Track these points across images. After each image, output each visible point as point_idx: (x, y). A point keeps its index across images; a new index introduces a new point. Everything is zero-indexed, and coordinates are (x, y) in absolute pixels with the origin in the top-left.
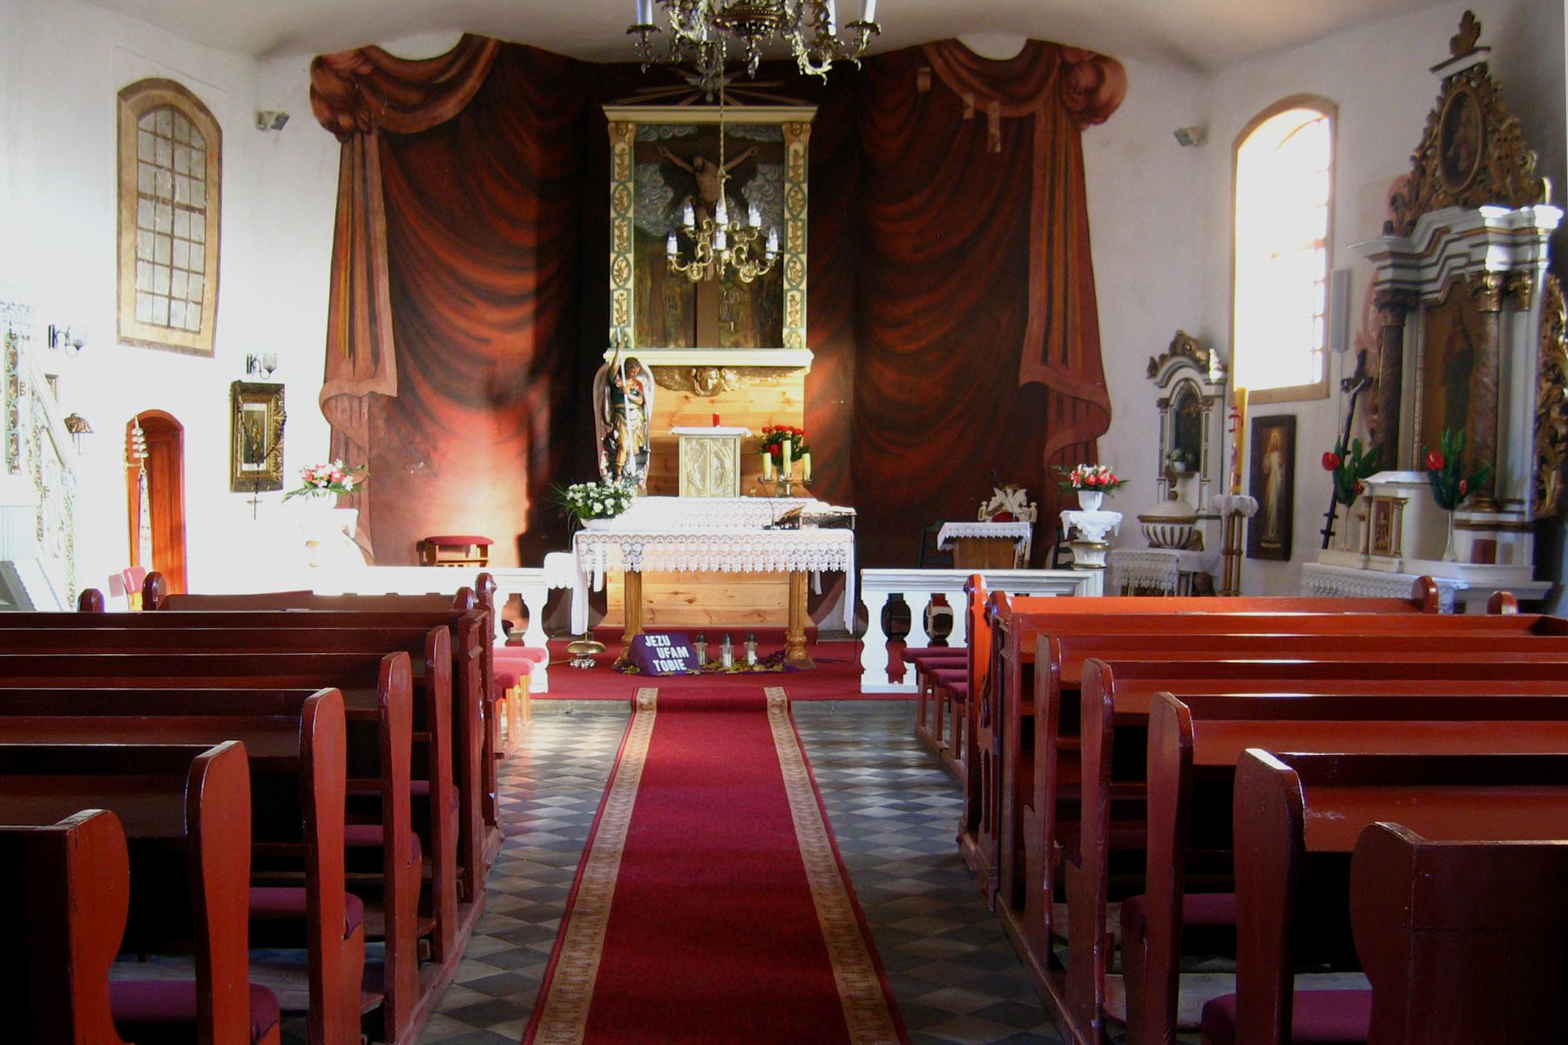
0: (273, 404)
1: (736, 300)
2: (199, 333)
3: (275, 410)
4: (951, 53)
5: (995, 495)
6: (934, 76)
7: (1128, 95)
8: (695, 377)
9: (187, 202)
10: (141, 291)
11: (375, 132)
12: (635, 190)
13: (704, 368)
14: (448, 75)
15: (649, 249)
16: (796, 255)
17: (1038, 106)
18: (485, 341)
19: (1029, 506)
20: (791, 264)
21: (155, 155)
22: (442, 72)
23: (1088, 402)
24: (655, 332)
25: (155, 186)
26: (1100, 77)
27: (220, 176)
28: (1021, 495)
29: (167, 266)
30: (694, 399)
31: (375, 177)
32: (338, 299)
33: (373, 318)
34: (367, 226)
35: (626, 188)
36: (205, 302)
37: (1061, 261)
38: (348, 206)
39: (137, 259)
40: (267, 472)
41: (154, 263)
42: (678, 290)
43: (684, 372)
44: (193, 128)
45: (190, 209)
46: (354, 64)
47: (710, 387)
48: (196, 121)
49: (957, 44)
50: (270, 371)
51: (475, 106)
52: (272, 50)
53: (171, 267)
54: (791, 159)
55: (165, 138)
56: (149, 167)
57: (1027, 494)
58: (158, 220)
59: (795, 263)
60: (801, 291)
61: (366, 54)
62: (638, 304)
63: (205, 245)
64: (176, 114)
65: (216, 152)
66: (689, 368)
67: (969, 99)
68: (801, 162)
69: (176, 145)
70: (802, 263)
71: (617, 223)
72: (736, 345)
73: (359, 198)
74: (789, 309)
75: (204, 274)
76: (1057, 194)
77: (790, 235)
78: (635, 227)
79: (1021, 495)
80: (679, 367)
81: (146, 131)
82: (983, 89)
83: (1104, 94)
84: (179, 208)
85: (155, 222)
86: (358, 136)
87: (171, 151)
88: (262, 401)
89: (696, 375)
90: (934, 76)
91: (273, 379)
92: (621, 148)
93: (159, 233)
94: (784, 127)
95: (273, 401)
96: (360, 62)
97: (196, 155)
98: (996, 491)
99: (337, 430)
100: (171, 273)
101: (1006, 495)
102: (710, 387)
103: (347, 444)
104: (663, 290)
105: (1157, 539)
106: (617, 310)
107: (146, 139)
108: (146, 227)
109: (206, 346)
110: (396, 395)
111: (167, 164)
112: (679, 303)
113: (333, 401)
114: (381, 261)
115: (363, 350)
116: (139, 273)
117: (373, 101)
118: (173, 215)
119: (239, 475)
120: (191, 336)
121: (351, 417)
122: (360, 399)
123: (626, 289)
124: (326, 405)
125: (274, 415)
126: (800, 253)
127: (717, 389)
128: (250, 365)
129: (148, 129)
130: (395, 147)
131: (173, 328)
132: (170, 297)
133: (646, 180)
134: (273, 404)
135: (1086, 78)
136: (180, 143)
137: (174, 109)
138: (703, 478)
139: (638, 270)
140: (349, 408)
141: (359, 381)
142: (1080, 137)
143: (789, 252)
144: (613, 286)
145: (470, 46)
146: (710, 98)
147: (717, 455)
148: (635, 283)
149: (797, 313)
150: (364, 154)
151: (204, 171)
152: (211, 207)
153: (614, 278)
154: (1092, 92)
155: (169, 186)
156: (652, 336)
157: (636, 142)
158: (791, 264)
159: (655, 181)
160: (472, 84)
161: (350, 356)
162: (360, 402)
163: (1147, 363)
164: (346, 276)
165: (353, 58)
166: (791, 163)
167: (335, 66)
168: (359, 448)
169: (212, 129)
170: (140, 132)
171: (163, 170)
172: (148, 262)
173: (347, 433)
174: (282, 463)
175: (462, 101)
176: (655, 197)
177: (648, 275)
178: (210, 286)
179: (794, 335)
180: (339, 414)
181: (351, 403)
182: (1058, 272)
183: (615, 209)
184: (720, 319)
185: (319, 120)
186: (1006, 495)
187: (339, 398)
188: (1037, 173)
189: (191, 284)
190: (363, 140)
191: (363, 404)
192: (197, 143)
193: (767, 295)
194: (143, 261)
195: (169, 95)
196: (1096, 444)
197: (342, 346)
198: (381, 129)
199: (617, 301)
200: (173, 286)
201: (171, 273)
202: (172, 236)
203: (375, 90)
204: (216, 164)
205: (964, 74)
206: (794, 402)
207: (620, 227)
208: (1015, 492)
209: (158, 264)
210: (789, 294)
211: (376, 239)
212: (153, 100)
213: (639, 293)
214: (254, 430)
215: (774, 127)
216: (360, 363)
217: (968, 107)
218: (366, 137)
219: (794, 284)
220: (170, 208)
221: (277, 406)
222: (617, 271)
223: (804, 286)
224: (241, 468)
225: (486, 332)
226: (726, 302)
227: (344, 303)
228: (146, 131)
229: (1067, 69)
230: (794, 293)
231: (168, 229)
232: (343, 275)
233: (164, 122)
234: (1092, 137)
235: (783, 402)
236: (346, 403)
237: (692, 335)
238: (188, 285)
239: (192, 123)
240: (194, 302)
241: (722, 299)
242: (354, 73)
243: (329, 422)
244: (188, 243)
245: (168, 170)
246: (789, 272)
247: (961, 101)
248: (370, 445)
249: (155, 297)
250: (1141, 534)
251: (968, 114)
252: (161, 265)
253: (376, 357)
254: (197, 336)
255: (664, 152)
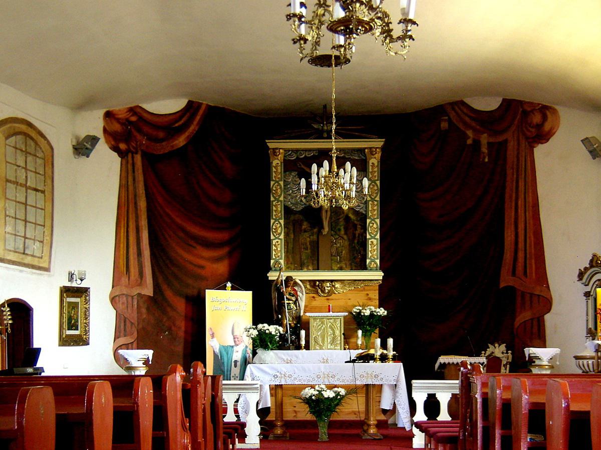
0: (83, 298)
1: (340, 245)
2: (41, 258)
3: (84, 302)
4: (460, 109)
5: (489, 348)
6: (450, 121)
7: (561, 126)
8: (318, 286)
9: (34, 186)
10: (8, 233)
11: (140, 152)
12: (284, 186)
13: (323, 281)
14: (180, 123)
15: (292, 218)
16: (374, 220)
17: (508, 135)
18: (202, 267)
19: (507, 353)
20: (371, 225)
21: (16, 159)
22: (177, 121)
23: (539, 295)
24: (296, 262)
25: (16, 176)
26: (545, 118)
27: (53, 173)
28: (503, 347)
29: (23, 220)
30: (318, 298)
31: (140, 177)
32: (120, 243)
33: (139, 254)
34: (136, 203)
35: (279, 185)
36: (45, 241)
37: (523, 219)
38: (125, 193)
39: (6, 216)
40: (80, 335)
41: (16, 218)
42: (308, 239)
43: (312, 284)
44: (37, 147)
45: (36, 190)
46: (127, 115)
47: (327, 291)
48: (39, 143)
49: (462, 103)
50: (82, 280)
51: (192, 141)
52: (82, 105)
53: (26, 221)
54: (370, 167)
55: (21, 150)
56: (13, 166)
57: (506, 347)
58: (18, 195)
59: (373, 224)
60: (377, 239)
61: (134, 110)
62: (286, 247)
63: (44, 210)
64: (28, 138)
65: (50, 161)
66: (315, 281)
67: (470, 133)
68: (376, 169)
69: (28, 155)
70: (377, 224)
71: (274, 203)
72: (341, 269)
73: (131, 188)
74: (370, 249)
75: (44, 226)
76: (520, 183)
77: (370, 209)
78: (284, 205)
79: (503, 347)
80: (310, 281)
81: (10, 146)
82: (478, 127)
83: (547, 127)
84: (30, 189)
85: (16, 196)
86: (130, 155)
87: (24, 158)
88: (77, 297)
89: (319, 285)
90: (450, 121)
91: (84, 285)
92: (277, 163)
93: (19, 202)
94: (366, 150)
95: (83, 297)
96: (131, 114)
97: (39, 161)
98: (490, 345)
99: (119, 314)
100: (26, 224)
101: (495, 348)
102: (327, 291)
103: (125, 322)
104: (300, 239)
105: (589, 368)
106: (275, 250)
107: (10, 150)
108: (10, 198)
109: (45, 265)
110: (152, 296)
111: (23, 165)
112: (309, 246)
113: (117, 298)
114: (144, 223)
115: (134, 270)
116: (7, 223)
117: (139, 137)
118: (26, 192)
119: (64, 336)
120: (37, 259)
121: (127, 307)
122: (132, 297)
123: (280, 239)
124: (113, 300)
125: (84, 305)
126: (376, 219)
127: (330, 293)
128: (71, 276)
129: (12, 145)
130: (151, 161)
131: (27, 254)
132: (25, 238)
133: (290, 180)
134: (83, 298)
135: (537, 118)
136: (30, 154)
137: (26, 135)
138: (323, 341)
139: (286, 229)
140: (126, 302)
141: (132, 288)
142: (533, 151)
143: (370, 218)
144: (272, 237)
145: (192, 107)
146: (325, 135)
147: (330, 327)
148: (284, 236)
149: (374, 251)
150: (133, 165)
151: (43, 170)
152: (48, 190)
153: (273, 234)
154: (540, 126)
155: (24, 177)
156: (295, 264)
157: (284, 160)
158: (371, 225)
159: (295, 181)
160: (193, 128)
161: (126, 274)
162: (133, 299)
163: (577, 273)
164: (124, 223)
165: (127, 112)
166: (370, 170)
167: (117, 116)
168: (132, 323)
169: (48, 147)
170: (7, 146)
171: (20, 168)
172: (12, 217)
173: (125, 315)
174: (89, 315)
175: (188, 136)
176: (295, 190)
177: (291, 231)
178: (47, 232)
179: (372, 263)
180: (121, 305)
181: (127, 299)
182: (521, 226)
183: (273, 196)
184: (331, 255)
185: (108, 146)
186: (495, 348)
187: (121, 296)
188: (509, 171)
189: (37, 231)
190: (133, 158)
191: (134, 300)
192: (40, 155)
193: (358, 242)
194: (10, 217)
195: (23, 127)
196: (544, 319)
197: (122, 268)
198: (142, 151)
199: (275, 245)
200: (27, 231)
201: (26, 224)
202: (26, 204)
203: (140, 131)
204: (50, 166)
205: (467, 119)
206: (373, 299)
207: (276, 206)
208: (499, 345)
209: (18, 219)
210: (370, 241)
211: (141, 211)
212: (14, 129)
213: (287, 241)
214: (73, 312)
215: (361, 151)
216: (132, 278)
217: (469, 138)
218: (134, 155)
219: (373, 235)
220: (24, 189)
221: (86, 299)
222: (275, 229)
223: (378, 237)
224: (65, 333)
225: (202, 262)
226: (335, 245)
227: (123, 245)
228: (10, 146)
229: (526, 114)
230: (373, 240)
231: (23, 200)
232: (122, 231)
233: (21, 142)
234: (540, 151)
235: (367, 299)
236: (125, 299)
237: (316, 264)
238: (35, 232)
239: (36, 143)
240: (38, 241)
241: (333, 244)
242: (127, 120)
243: (115, 309)
244: (35, 209)
245: (23, 168)
246: (370, 229)
247: (465, 134)
248: (138, 322)
249: (17, 237)
250: (575, 365)
251: (469, 142)
252: (20, 219)
253: (141, 274)
254: (40, 260)
255: (300, 165)
